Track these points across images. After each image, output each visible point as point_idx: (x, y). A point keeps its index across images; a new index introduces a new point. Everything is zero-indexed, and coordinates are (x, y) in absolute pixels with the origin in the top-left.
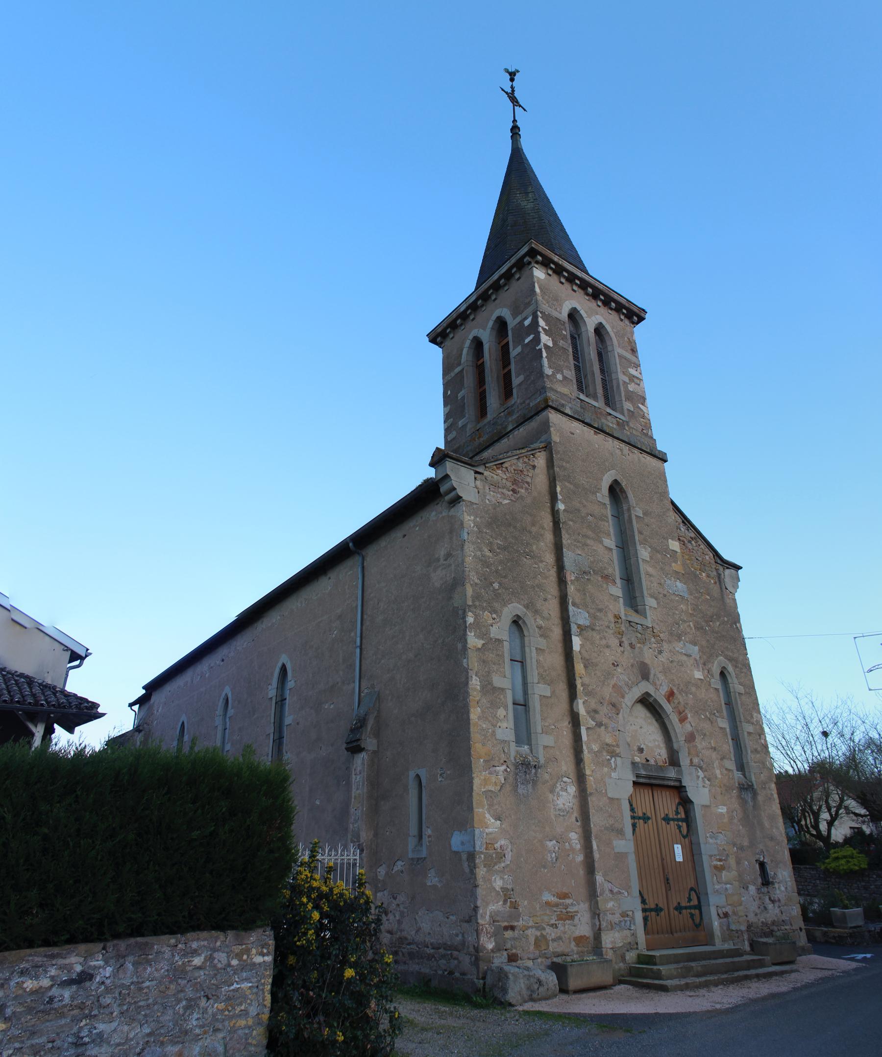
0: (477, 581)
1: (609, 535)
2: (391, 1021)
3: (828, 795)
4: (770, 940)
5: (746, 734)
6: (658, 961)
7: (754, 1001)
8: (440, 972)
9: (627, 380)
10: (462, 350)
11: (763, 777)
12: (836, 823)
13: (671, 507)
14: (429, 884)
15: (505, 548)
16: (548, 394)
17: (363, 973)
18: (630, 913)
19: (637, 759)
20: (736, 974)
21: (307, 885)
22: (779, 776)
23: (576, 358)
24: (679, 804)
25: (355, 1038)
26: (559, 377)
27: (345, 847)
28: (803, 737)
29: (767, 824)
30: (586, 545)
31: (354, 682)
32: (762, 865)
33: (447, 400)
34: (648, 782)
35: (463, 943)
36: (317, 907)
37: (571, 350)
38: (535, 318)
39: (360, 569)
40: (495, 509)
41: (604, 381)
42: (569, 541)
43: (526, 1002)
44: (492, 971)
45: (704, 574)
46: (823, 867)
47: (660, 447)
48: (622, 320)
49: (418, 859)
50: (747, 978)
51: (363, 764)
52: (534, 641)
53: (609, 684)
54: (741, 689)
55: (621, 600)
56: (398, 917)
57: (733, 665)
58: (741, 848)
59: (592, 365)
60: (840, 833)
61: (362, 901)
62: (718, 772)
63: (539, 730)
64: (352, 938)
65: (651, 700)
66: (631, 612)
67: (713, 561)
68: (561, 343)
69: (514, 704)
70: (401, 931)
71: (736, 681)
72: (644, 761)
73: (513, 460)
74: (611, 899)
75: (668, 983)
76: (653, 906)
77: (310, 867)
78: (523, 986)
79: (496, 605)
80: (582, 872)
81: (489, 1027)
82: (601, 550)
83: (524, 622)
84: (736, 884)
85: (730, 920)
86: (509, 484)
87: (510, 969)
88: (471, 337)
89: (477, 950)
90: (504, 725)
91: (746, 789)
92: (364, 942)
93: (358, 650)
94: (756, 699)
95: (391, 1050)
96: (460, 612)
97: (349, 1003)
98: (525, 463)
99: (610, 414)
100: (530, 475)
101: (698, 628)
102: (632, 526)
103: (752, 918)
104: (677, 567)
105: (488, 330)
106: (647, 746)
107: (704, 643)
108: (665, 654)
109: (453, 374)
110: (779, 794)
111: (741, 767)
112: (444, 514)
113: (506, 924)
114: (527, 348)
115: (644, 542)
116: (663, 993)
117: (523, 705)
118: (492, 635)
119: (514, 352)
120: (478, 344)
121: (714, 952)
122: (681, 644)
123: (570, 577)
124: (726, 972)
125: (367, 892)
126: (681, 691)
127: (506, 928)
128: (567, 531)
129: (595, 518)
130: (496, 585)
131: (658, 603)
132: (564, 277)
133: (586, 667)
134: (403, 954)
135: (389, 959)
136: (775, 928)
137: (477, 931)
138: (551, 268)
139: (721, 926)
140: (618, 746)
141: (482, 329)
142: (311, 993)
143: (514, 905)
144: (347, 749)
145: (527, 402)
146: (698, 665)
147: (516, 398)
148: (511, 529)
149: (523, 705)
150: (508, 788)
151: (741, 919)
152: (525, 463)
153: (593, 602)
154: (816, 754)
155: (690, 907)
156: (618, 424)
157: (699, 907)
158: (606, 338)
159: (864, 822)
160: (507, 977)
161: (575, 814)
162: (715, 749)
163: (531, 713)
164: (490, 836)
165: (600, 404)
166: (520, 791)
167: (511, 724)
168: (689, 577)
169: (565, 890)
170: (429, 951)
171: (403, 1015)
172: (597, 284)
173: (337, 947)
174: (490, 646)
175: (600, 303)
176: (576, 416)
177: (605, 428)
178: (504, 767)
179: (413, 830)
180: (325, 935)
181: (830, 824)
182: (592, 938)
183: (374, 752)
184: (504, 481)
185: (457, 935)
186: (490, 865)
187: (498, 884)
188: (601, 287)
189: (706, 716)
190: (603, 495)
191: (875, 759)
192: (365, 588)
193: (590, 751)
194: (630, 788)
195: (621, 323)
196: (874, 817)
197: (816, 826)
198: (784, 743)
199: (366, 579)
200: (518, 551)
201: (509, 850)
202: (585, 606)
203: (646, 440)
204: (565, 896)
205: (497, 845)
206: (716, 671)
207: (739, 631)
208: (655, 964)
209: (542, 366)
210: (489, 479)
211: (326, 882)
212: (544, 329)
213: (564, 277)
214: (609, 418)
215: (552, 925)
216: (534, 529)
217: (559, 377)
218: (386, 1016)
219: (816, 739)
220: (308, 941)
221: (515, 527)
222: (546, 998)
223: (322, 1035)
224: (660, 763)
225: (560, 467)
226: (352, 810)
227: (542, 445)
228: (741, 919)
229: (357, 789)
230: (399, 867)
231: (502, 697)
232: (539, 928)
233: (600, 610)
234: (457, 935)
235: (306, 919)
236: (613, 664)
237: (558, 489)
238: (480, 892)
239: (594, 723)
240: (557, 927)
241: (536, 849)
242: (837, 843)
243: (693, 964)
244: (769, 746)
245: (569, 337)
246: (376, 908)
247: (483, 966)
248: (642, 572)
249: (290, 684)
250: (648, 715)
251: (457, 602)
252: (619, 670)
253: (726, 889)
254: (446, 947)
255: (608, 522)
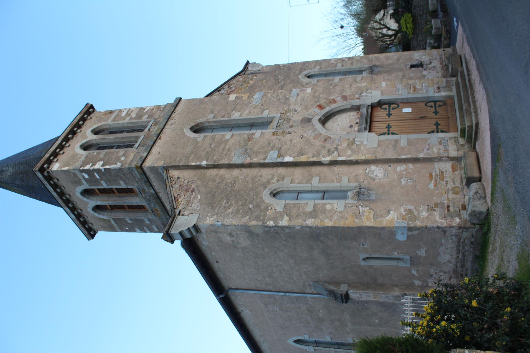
0: (248, 218)
1: (224, 135)
2: (499, 279)
3: (373, 29)
4: (450, 67)
5: (342, 68)
6: (463, 127)
7: (481, 78)
8: (472, 250)
9: (128, 118)
10: (100, 219)
11: (366, 61)
12: (388, 26)
13: (209, 97)
14: (424, 255)
15: (228, 200)
16: (133, 166)
17: (474, 295)
18: (439, 140)
19: (356, 129)
20: (468, 86)
21: (426, 329)
22: (365, 53)
23: (112, 147)
24: (381, 107)
25: (508, 301)
26: (123, 158)
27: (403, 305)
28: (344, 38)
29: (391, 62)
30: (229, 150)
31: (307, 297)
32: (412, 66)
33: (132, 230)
34: (369, 124)
35: (456, 236)
36: (438, 323)
37: (106, 151)
38: (83, 171)
39: (237, 291)
40: (203, 204)
41: (128, 131)
42: (226, 159)
43: (486, 201)
44: (471, 219)
45: (251, 82)
46: (411, 35)
47: (172, 101)
48: (91, 118)
49: (411, 260)
50: (470, 80)
51: (355, 293)
52: (286, 184)
53: (313, 142)
54: (317, 68)
55: (264, 131)
56: (442, 274)
57: (304, 71)
58: (404, 76)
59: (117, 138)
60: (393, 25)
61: (435, 295)
62: (363, 85)
63: (339, 185)
64: (455, 302)
65: (323, 118)
66: (271, 125)
67: (243, 76)
68: (102, 156)
69: (323, 199)
70: (450, 272)
71: (313, 70)
72: (357, 125)
73: (173, 190)
74: (432, 150)
75: (474, 122)
76: (435, 127)
77: (415, 327)
78: (478, 202)
79: (263, 206)
80: (418, 165)
81: (500, 223)
82: (232, 141)
83: (274, 190)
84: (422, 81)
85: (441, 86)
86: (188, 194)
87: (470, 209)
88: (92, 212)
89: (460, 228)
90: (335, 206)
91: (372, 70)
92: (457, 294)
93: (287, 294)
94: (323, 60)
95: (514, 280)
96: (266, 229)
97: (490, 304)
98: (175, 183)
99: (149, 129)
100: (183, 180)
101: (282, 88)
102: (219, 121)
103: (440, 74)
104: (245, 97)
105: (89, 201)
106: (349, 123)
107: (291, 85)
108: (297, 108)
109: (115, 225)
110: (374, 54)
111: (360, 72)
112: (204, 236)
113: (446, 210)
114: (103, 176)
115: (229, 115)
116: (479, 125)
117: (324, 194)
118: (282, 210)
119: (104, 185)
120: (98, 208)
121: (458, 96)
122: (291, 98)
123: (248, 160)
124: (468, 91)
125: (430, 292)
126: (318, 101)
127: (448, 210)
128: (220, 160)
129: (212, 143)
130: (251, 206)
131: (266, 109)
132: (60, 151)
133: (303, 155)
134: (462, 271)
135: (466, 280)
136: (444, 63)
137: (450, 227)
138: (53, 159)
139: (445, 91)
140: (349, 139)
141: (88, 205)
142: (485, 326)
143: (437, 205)
144: (347, 302)
145: (137, 179)
146: (303, 90)
147: (134, 186)
148: (217, 194)
149: (324, 194)
150: (372, 205)
151: (440, 80)
152: (175, 183)
153: (264, 147)
154: (353, 33)
155: (435, 106)
156: (155, 125)
157: (435, 102)
158: (101, 128)
159: (387, 13)
160: (474, 211)
161: (387, 166)
162: (351, 86)
163: (329, 189)
164: (399, 217)
165: (142, 135)
166: (374, 198)
167: (335, 201)
168: (252, 90)
169: (428, 175)
170: (460, 255)
171: (495, 273)
172: (67, 131)
173: (460, 311)
174: (288, 212)
175: (79, 131)
176: (148, 150)
177: (158, 133)
178: (360, 207)
179: (394, 263)
180: (453, 318)
181: (389, 29)
182: (453, 162)
183: (349, 286)
184: (186, 197)
185: (452, 239)
186: (414, 218)
187: (425, 214)
188: (69, 129)
189: (333, 88)
190: (199, 137)
191: (354, 5)
192: (248, 288)
193: (351, 155)
194: (372, 134)
195: (93, 118)
196: (385, 7)
197: (390, 36)
198: (347, 48)
199: (243, 288)
200: (230, 191)
201: (406, 207)
202: (266, 152)
203: (167, 109)
204: (431, 175)
205: (404, 213)
206: (307, 80)
207: (284, 66)
208: (465, 128)
209: (115, 169)
210: (184, 206)
211: (424, 317)
212: (92, 166)
213: (60, 151)
214: (151, 130)
215: (447, 184)
216: (218, 180)
217: (123, 158)
218: (498, 282)
219: (344, 32)
220: (457, 328)
221: (216, 192)
222: (484, 190)
223: (508, 320)
224: (359, 116)
225: (180, 162)
226: (382, 300)
227: (165, 172)
228: (440, 80)
229: (370, 297)
230: (415, 272)
231: (319, 206)
232: (447, 192)
233: (269, 144)
234: (452, 239)
235: (445, 330)
236: (302, 138)
237: (193, 164)
238: (429, 225)
239: (336, 152)
240: (447, 181)
241: (403, 190)
242: (398, 27)
243: (464, 108)
244: (349, 56)
245: (98, 151)
246: (439, 287)
247: (468, 225)
248: (247, 117)
249: (306, 337)
250: (331, 120)
251: (260, 231)
252: (305, 135)
253: (425, 86)
254: (458, 246)
255: (216, 135)
